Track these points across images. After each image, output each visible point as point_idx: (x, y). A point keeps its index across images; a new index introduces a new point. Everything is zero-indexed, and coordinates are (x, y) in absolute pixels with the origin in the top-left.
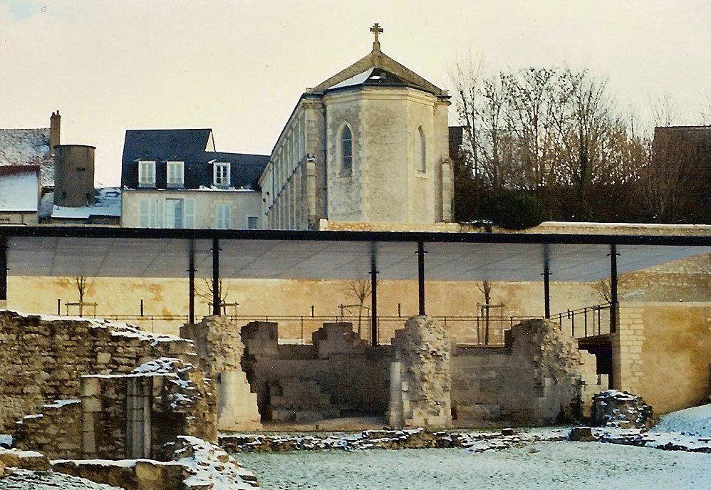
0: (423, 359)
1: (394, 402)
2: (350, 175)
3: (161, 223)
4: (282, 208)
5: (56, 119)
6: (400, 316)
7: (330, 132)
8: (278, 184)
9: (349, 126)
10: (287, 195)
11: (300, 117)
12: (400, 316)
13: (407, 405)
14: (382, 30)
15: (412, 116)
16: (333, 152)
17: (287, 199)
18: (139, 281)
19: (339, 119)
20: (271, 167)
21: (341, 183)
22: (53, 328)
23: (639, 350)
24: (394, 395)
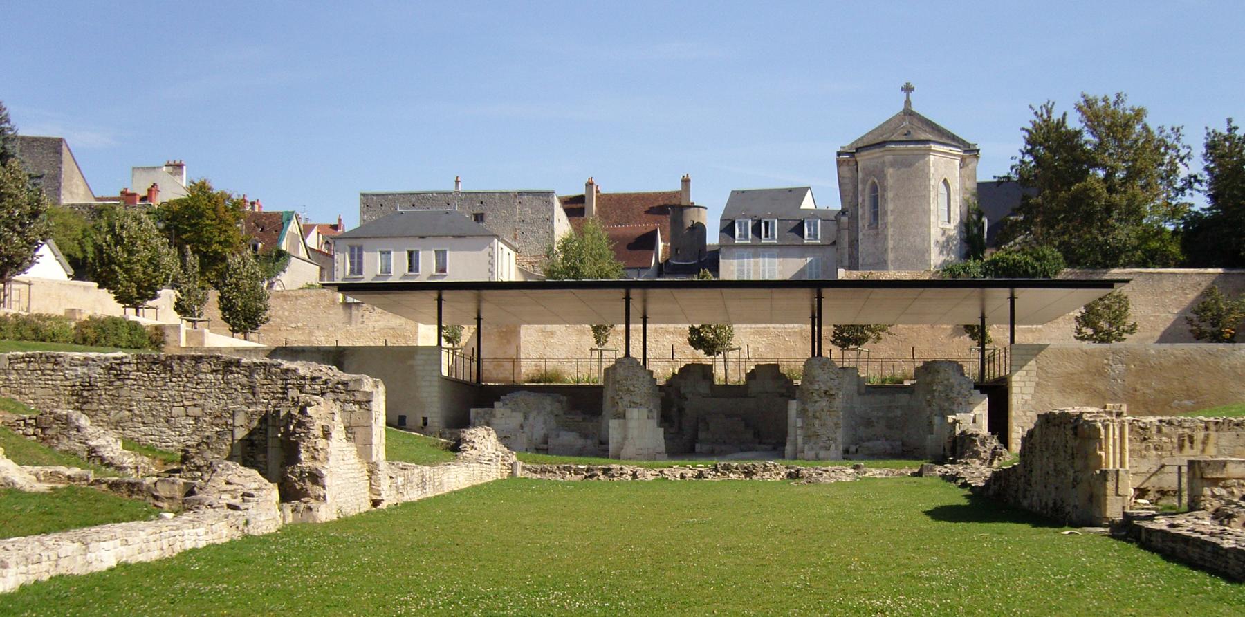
0: (817, 398)
1: (790, 438)
2: (877, 227)
3: (756, 272)
5: (686, 182)
7: (860, 187)
13: (800, 440)
14: (913, 89)
15: (936, 170)
16: (863, 206)
18: (671, 327)
19: (869, 173)
22: (251, 369)
23: (1032, 391)
24: (791, 430)
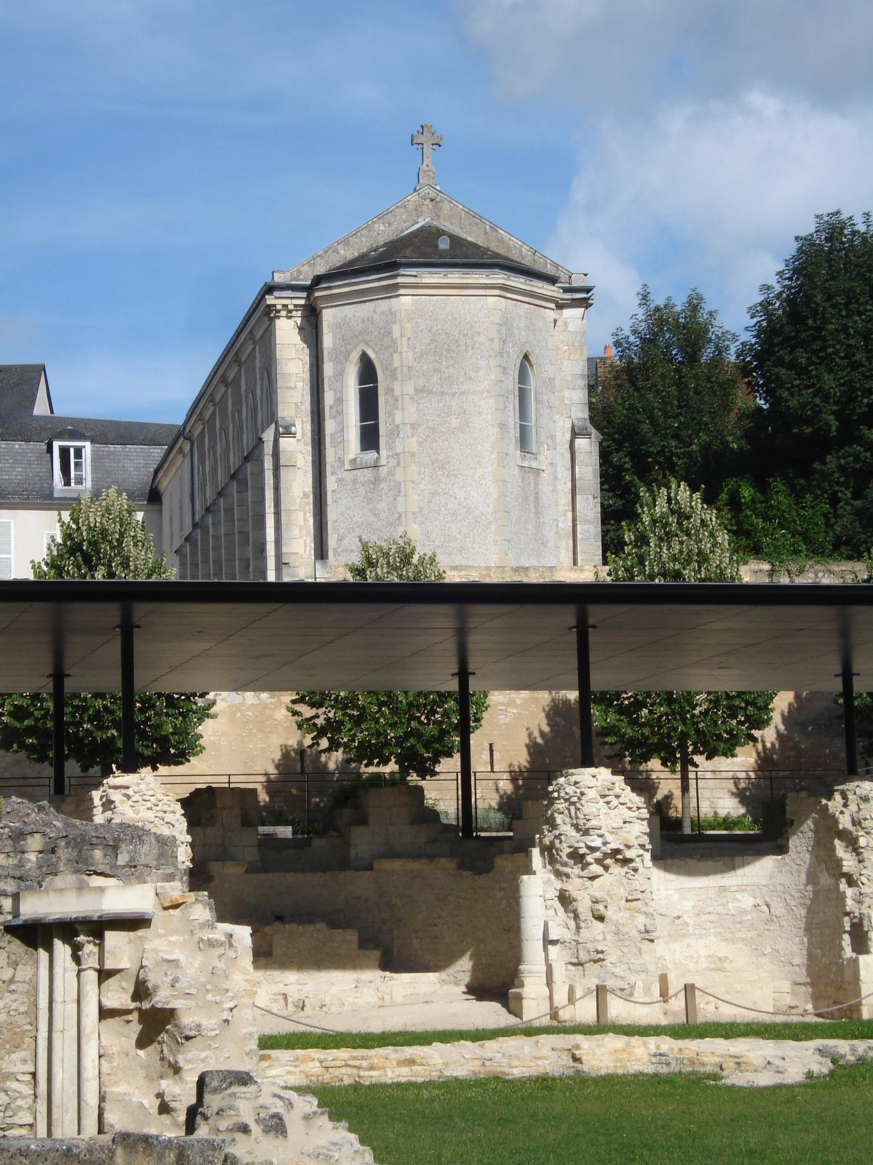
4: (217, 538)
6: (492, 771)
8: (203, 486)
9: (372, 355)
10: (229, 510)
11: (258, 335)
12: (492, 771)
16: (339, 413)
17: (230, 520)
20: (187, 448)
21: (355, 481)
